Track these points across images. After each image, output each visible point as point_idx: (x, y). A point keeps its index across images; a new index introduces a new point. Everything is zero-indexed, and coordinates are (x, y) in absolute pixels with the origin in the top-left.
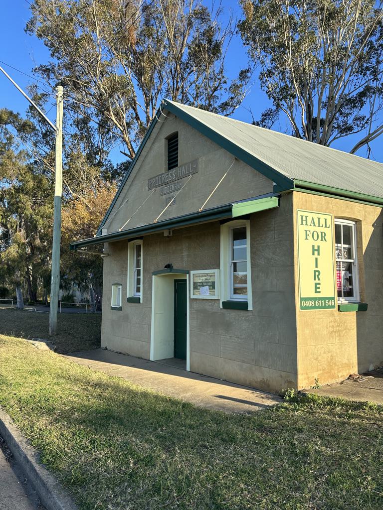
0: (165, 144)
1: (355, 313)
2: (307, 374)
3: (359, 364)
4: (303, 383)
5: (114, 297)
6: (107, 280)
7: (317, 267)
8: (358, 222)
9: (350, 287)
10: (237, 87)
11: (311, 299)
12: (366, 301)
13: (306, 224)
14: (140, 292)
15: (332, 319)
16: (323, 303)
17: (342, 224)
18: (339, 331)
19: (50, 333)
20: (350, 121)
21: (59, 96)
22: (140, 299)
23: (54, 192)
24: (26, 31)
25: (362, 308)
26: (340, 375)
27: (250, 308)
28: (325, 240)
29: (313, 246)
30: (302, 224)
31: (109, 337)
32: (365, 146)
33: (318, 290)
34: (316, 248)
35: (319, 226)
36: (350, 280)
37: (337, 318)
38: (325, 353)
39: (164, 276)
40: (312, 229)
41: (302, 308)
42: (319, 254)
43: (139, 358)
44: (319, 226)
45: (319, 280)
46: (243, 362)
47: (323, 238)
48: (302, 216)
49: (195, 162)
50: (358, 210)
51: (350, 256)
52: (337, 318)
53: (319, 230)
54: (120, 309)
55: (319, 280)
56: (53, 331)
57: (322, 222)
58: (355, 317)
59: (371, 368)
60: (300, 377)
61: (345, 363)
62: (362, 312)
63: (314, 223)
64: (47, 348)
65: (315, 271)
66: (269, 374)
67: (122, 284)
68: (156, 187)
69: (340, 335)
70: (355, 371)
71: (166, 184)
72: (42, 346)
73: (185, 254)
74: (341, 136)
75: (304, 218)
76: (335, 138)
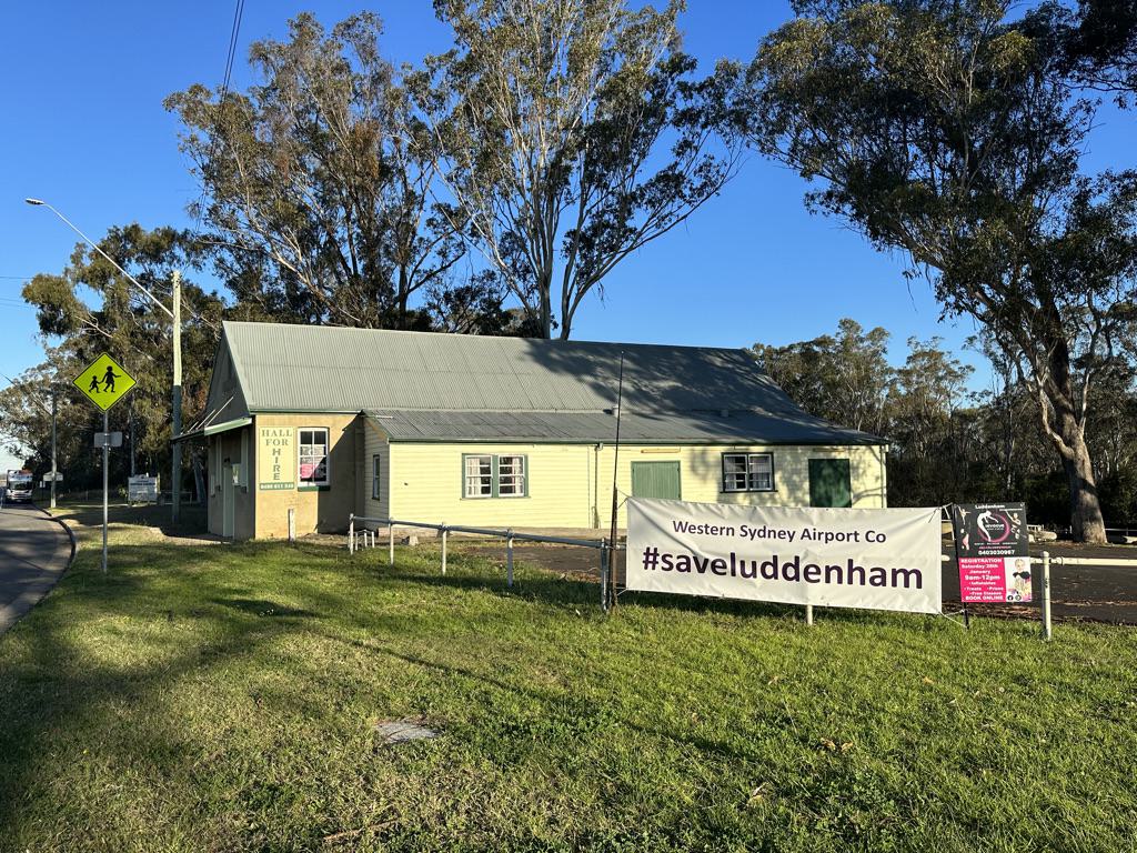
1: (317, 493)
25: (322, 489)
36: (324, 470)
40: (273, 438)
57: (284, 432)
64: (160, 532)
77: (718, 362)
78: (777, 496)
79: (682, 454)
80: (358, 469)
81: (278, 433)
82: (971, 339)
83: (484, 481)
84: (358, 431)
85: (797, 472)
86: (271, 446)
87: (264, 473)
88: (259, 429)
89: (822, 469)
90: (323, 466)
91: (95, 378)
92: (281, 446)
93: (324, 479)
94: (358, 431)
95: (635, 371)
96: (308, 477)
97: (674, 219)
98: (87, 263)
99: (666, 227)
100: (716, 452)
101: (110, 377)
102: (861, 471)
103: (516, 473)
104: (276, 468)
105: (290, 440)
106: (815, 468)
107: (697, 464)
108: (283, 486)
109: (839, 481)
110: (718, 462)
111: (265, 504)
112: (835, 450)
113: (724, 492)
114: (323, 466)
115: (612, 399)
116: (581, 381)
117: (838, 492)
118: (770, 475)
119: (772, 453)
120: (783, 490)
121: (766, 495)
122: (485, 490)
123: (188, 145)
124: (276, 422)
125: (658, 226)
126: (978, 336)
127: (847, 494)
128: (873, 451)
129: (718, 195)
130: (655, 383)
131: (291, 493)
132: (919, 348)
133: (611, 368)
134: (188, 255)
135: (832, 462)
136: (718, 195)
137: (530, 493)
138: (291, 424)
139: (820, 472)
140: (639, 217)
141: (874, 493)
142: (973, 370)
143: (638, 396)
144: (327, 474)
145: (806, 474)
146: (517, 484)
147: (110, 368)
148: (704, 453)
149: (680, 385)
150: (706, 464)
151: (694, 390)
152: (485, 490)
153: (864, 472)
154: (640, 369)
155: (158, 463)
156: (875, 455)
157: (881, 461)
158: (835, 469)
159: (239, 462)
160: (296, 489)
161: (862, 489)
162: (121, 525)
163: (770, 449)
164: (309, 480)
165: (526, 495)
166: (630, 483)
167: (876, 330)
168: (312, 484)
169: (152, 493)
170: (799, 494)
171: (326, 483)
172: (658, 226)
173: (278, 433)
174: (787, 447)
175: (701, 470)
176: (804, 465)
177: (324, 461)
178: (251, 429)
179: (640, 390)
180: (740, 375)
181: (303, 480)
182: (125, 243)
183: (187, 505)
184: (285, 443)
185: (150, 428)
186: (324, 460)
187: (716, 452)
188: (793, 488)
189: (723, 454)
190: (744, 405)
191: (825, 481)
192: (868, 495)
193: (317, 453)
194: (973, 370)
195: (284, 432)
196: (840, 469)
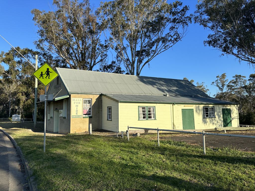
1: (88, 118)
8: (92, 99)
11: (75, 116)
14: (143, 118)
22: (66, 117)
23: (35, 86)
24: (33, 20)
25: (90, 117)
26: (83, 131)
32: (147, 64)
34: (77, 105)
36: (90, 111)
38: (78, 126)
40: (76, 102)
41: (72, 118)
50: (91, 96)
53: (78, 102)
56: (35, 127)
57: (79, 100)
60: (71, 131)
64: (32, 131)
66: (64, 131)
72: (30, 130)
74: (145, 58)
75: (74, 100)
76: (157, 54)
77: (183, 83)
78: (216, 119)
79: (193, 107)
80: (100, 111)
81: (77, 100)
82: (213, 83)
83: (144, 114)
84: (100, 100)
85: (219, 112)
87: (73, 112)
88: (72, 99)
89: (225, 111)
90: (90, 110)
91: (42, 72)
92: (78, 104)
93: (90, 114)
94: (100, 100)
95: (165, 85)
96: (85, 113)
97: (168, 47)
98: (4, 57)
99: (167, 49)
100: (202, 106)
101: (48, 73)
102: (233, 112)
103: (152, 112)
104: (77, 111)
105: (81, 102)
106: (223, 110)
107: (197, 110)
109: (228, 114)
110: (202, 109)
111: (73, 122)
112: (228, 106)
113: (204, 118)
114: (90, 110)
115: (164, 92)
116: (154, 87)
117: (228, 118)
118: (213, 113)
119: (214, 107)
120: (217, 117)
121: (213, 119)
122: (144, 118)
123: (37, 23)
125: (164, 48)
126: (215, 82)
127: (230, 118)
128: (235, 106)
129: (181, 40)
130: (172, 88)
131: (81, 119)
132: (199, 85)
133: (160, 84)
134: (32, 56)
135: (227, 109)
136: (181, 40)
137: (157, 118)
138: (81, 97)
139: (225, 112)
141: (236, 118)
142: (209, 90)
143: (169, 91)
144: (91, 113)
145: (221, 113)
146: (152, 116)
147: (48, 69)
148: (199, 107)
149: (178, 89)
150: (199, 110)
151: (182, 90)
152: (144, 118)
153: (234, 112)
154: (166, 84)
156: (236, 108)
157: (237, 109)
158: (228, 111)
159: (62, 109)
161: (233, 117)
162: (16, 128)
163: (214, 105)
164: (86, 114)
165: (155, 119)
166: (194, 116)
167: (192, 80)
168: (87, 116)
169: (18, 119)
170: (220, 118)
172: (164, 48)
173: (77, 100)
174: (217, 105)
175: (198, 111)
176: (221, 110)
177: (90, 109)
178: (68, 100)
179: (169, 90)
180: (190, 87)
181: (84, 115)
182: (14, 52)
183: (31, 122)
184: (79, 103)
185: (21, 101)
186: (90, 108)
187: (202, 106)
188: (219, 117)
189: (203, 107)
190: (195, 94)
191: (226, 115)
192: (235, 118)
193: (88, 106)
194: (209, 90)
195: (79, 100)
196: (229, 111)
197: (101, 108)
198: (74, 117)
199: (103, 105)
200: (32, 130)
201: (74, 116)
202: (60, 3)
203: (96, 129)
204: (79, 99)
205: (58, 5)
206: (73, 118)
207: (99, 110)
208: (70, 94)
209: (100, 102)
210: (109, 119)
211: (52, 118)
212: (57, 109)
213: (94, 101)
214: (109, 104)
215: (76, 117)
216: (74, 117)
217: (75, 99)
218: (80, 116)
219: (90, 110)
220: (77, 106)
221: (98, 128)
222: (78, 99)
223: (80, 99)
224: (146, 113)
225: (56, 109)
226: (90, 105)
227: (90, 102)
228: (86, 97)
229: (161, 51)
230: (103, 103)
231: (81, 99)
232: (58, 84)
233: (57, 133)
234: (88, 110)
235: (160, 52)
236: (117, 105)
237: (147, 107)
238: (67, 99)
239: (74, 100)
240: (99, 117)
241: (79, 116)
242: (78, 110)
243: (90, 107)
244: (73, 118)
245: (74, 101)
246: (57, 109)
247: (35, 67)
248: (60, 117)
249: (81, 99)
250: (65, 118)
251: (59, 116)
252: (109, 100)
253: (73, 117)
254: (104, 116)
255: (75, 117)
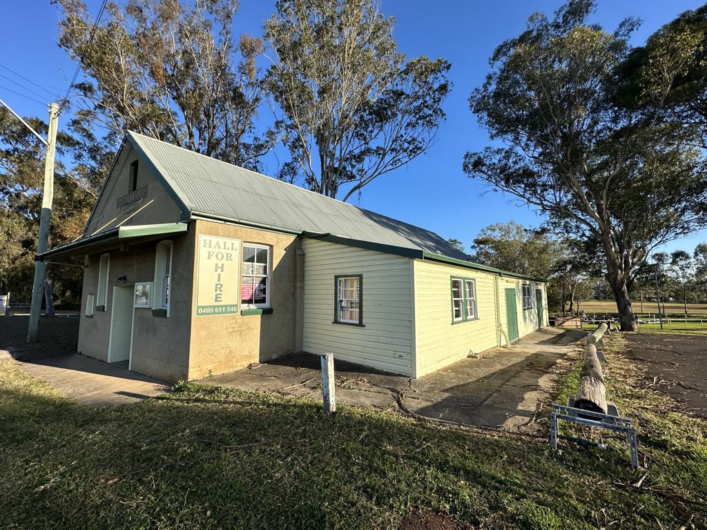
0: (130, 170)
2: (199, 367)
3: (261, 355)
4: (194, 374)
5: (88, 306)
6: (86, 288)
7: (219, 280)
8: (271, 246)
9: (264, 296)
10: (273, 133)
11: (210, 307)
12: (274, 307)
13: (210, 247)
15: (234, 321)
16: (220, 310)
17: (256, 248)
18: (241, 331)
19: (28, 341)
20: (355, 172)
21: (53, 113)
22: (166, 311)
24: (60, 46)
25: (266, 312)
26: (238, 365)
27: (168, 316)
28: (231, 260)
29: (217, 264)
30: (205, 246)
31: (86, 343)
33: (219, 299)
34: (220, 266)
35: (225, 248)
36: (264, 291)
37: (239, 321)
39: (126, 287)
41: (198, 314)
42: (222, 271)
43: (88, 357)
44: (225, 248)
45: (221, 291)
46: (161, 360)
47: (229, 257)
48: (205, 241)
49: (146, 187)
50: (270, 237)
51: (265, 273)
52: (239, 321)
53: (224, 252)
54: (92, 316)
55: (221, 291)
56: (31, 338)
57: (229, 245)
58: (260, 319)
59: (274, 356)
60: (190, 370)
61: (246, 355)
62: (265, 315)
63: (219, 246)
64: (9, 356)
65: (217, 285)
67: (94, 294)
68: (122, 206)
69: (241, 334)
70: (256, 359)
71: (128, 204)
73: (135, 266)
74: (342, 183)
75: (208, 242)
76: (380, 173)
80: (298, 291)
86: (214, 260)
90: (262, 287)
92: (224, 261)
93: (263, 301)
104: (219, 287)
105: (237, 255)
108: (226, 309)
124: (221, 232)
125: (392, 165)
137: (479, 315)
138: (235, 236)
140: (369, 163)
155: (178, 94)
160: (239, 313)
164: (249, 302)
168: (253, 306)
171: (266, 305)
172: (392, 165)
177: (263, 281)
178: (182, 245)
181: (244, 302)
195: (229, 245)
197: (303, 281)
198: (206, 314)
199: (306, 269)
200: (12, 353)
201: (206, 307)
202: (146, 12)
203: (285, 352)
204: (229, 242)
205: (142, 20)
206: (203, 314)
207: (295, 288)
208: (193, 217)
209: (298, 259)
210: (342, 320)
211: (104, 311)
212: (125, 278)
213: (279, 255)
214: (346, 265)
215: (214, 313)
216: (206, 314)
217: (215, 240)
218: (231, 306)
219: (265, 284)
220: (219, 270)
221: (290, 350)
222: (225, 243)
223: (233, 244)
224: (463, 299)
225: (120, 279)
226: (265, 267)
227: (262, 257)
228: (251, 238)
229: (387, 168)
230: (306, 264)
231: (237, 243)
232: (134, 188)
233: (120, 369)
234: (257, 285)
235: (384, 171)
236: (407, 266)
237: (464, 279)
238: (176, 237)
239: (208, 242)
240: (294, 313)
241: (226, 306)
242: (222, 286)
243: (265, 273)
244: (203, 314)
245: (209, 250)
246: (125, 278)
247: (47, 140)
248: (136, 308)
249: (237, 243)
250: (161, 313)
251: (135, 306)
252: (349, 257)
253: (201, 311)
254: (309, 306)
255: (210, 314)
